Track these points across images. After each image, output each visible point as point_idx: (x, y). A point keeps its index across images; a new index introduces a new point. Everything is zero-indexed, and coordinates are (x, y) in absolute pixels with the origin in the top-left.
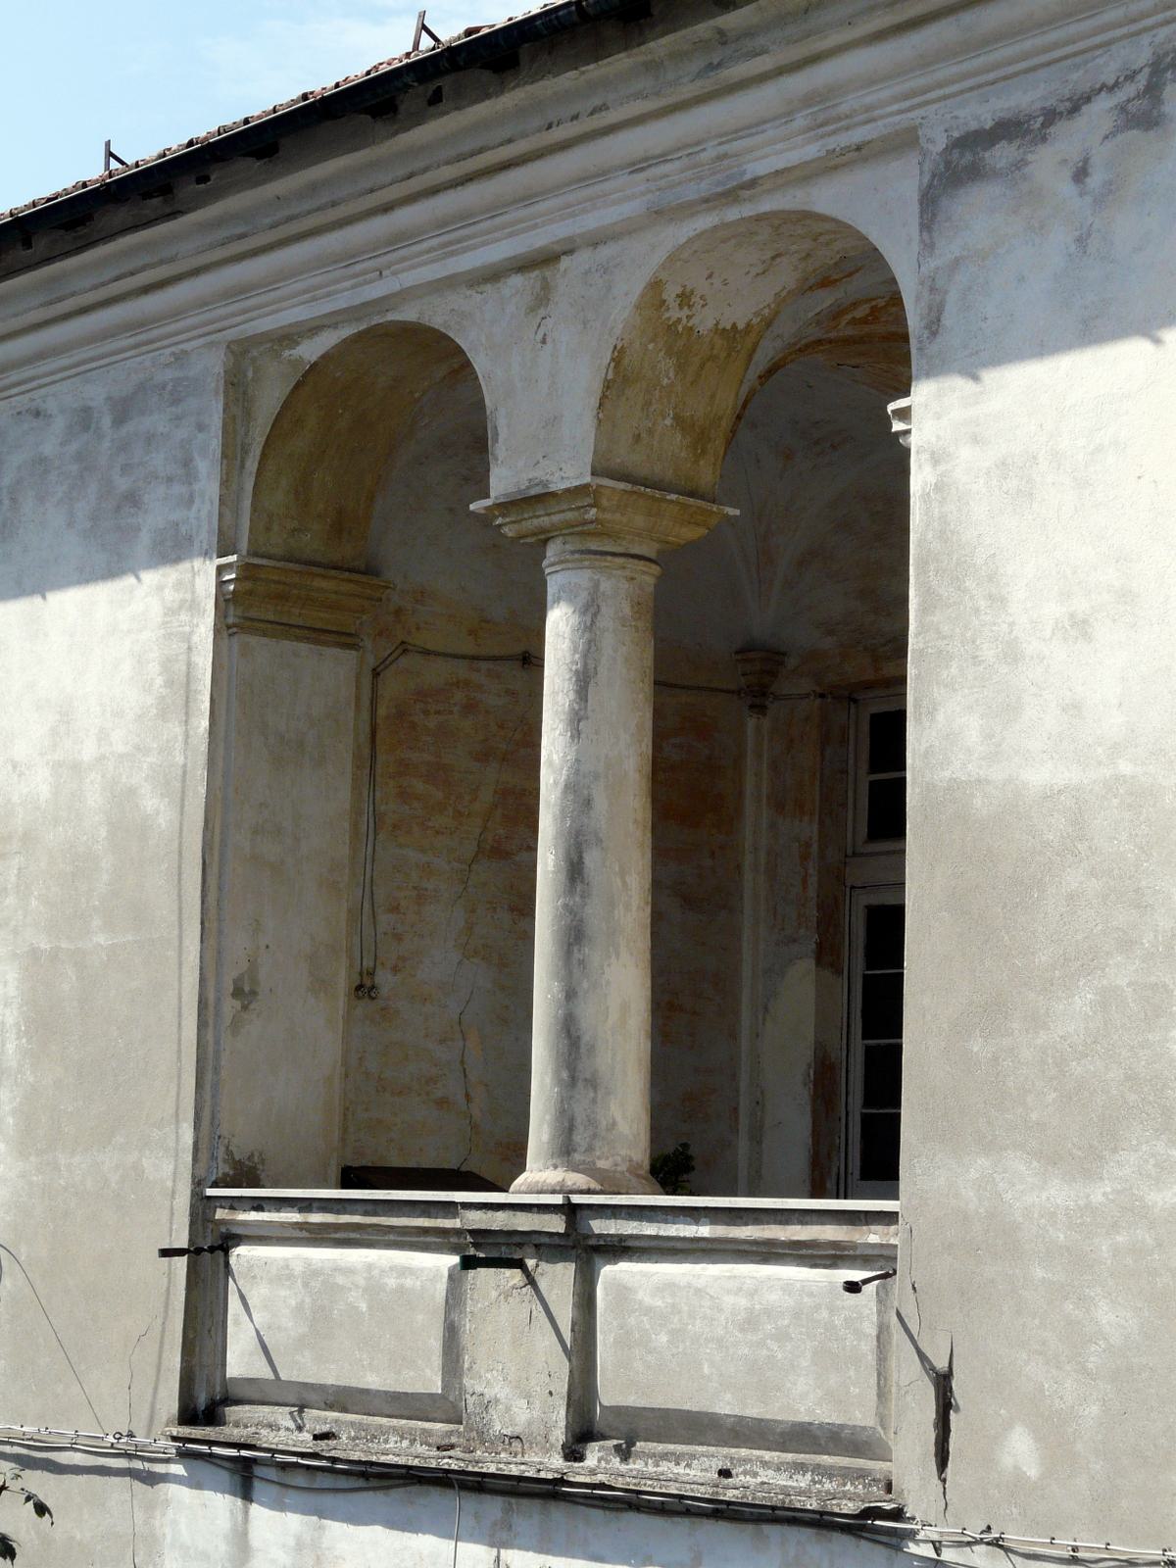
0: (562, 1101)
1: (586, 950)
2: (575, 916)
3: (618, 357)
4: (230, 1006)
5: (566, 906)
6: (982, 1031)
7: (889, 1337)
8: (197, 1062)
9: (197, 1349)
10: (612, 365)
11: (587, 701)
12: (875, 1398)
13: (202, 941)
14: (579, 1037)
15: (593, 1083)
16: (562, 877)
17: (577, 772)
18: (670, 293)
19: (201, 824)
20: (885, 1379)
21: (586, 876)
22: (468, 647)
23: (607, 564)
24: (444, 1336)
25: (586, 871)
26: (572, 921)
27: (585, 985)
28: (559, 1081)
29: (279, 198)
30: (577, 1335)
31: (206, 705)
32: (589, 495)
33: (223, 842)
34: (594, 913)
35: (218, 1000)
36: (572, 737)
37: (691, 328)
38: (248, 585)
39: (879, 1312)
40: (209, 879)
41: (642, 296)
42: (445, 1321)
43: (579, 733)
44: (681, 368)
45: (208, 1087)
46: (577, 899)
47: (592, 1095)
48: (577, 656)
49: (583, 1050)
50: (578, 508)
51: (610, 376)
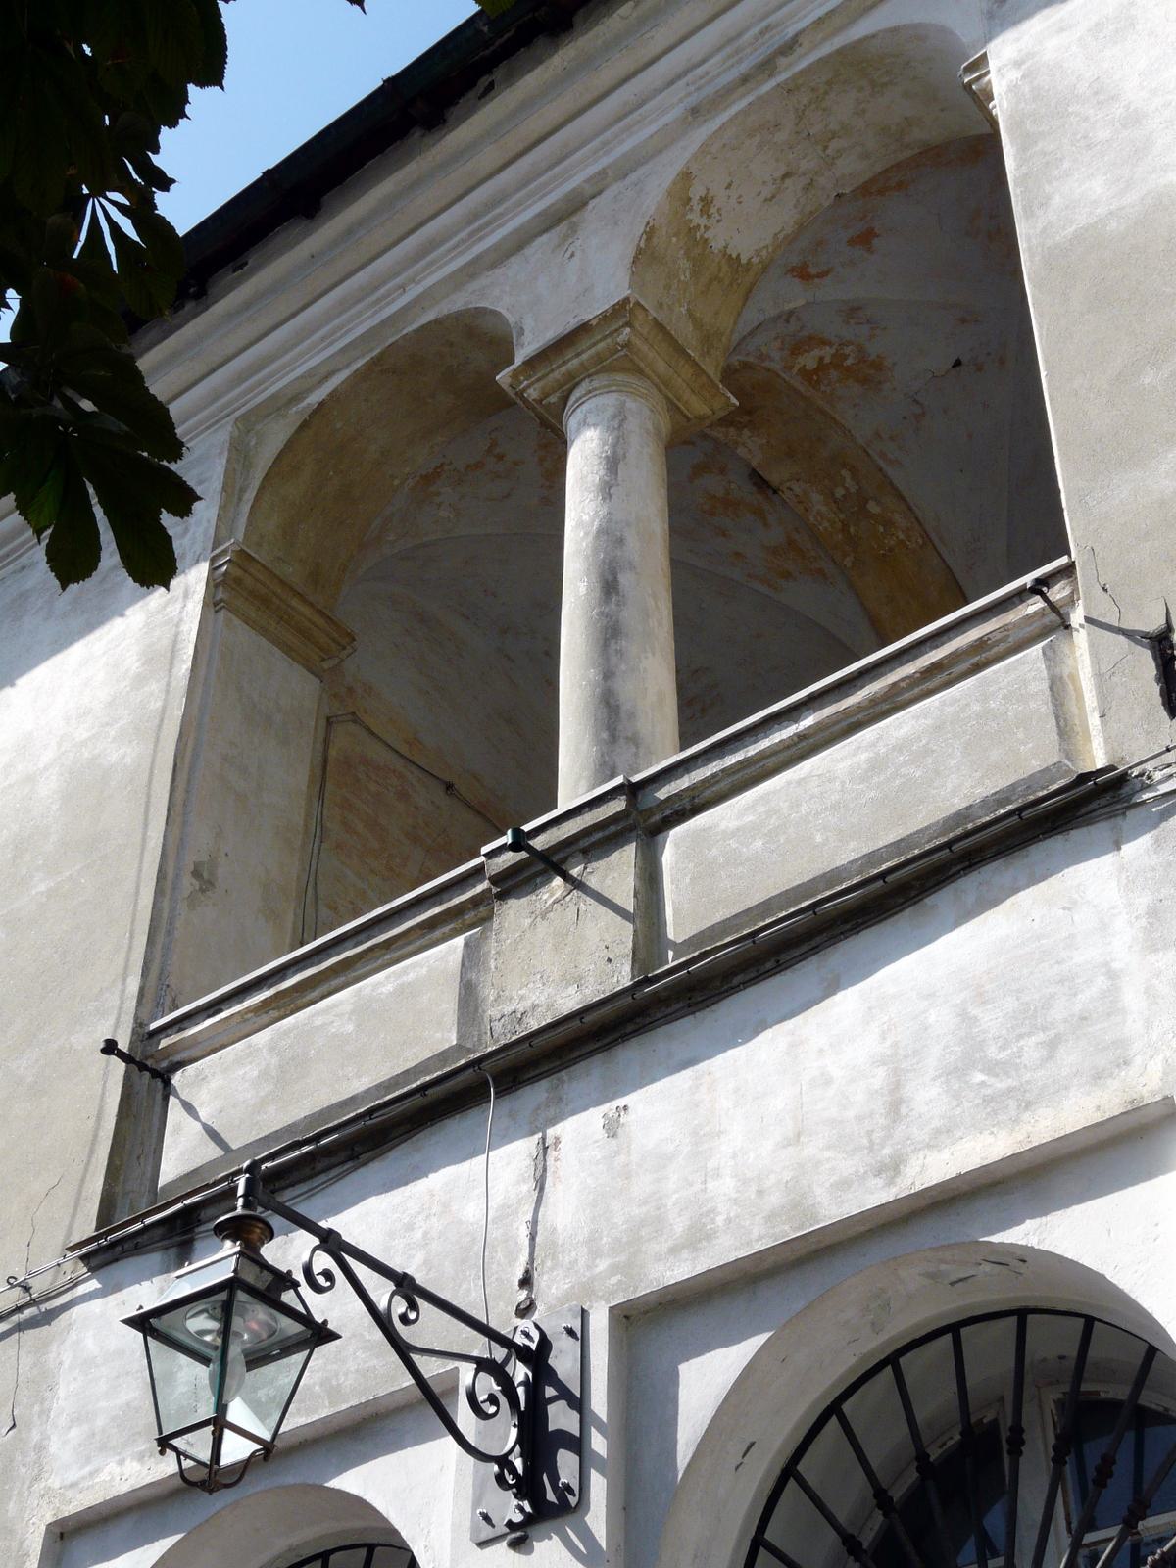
0: (602, 755)
1: (624, 642)
2: (611, 618)
3: (650, 233)
4: (188, 883)
5: (601, 613)
6: (1144, 389)
7: (1064, 687)
8: (151, 921)
9: (122, 1178)
10: (644, 237)
11: (617, 474)
12: (1057, 737)
13: (167, 824)
14: (618, 706)
15: (634, 740)
16: (597, 593)
17: (610, 521)
18: (697, 191)
19: (177, 736)
20: (1065, 720)
21: (621, 590)
22: (404, 749)
23: (632, 390)
24: (459, 994)
25: (621, 587)
26: (608, 622)
27: (623, 667)
28: (598, 741)
29: (312, 256)
30: (640, 904)
31: (191, 651)
32: (626, 316)
33: (196, 755)
34: (629, 616)
35: (177, 876)
36: (604, 499)
37: (706, 240)
38: (238, 573)
39: (1048, 668)
40: (178, 779)
41: (674, 183)
42: (461, 981)
43: (610, 496)
44: (695, 274)
45: (159, 946)
46: (613, 606)
47: (634, 750)
48: (606, 447)
49: (623, 715)
50: (611, 334)
51: (642, 245)
